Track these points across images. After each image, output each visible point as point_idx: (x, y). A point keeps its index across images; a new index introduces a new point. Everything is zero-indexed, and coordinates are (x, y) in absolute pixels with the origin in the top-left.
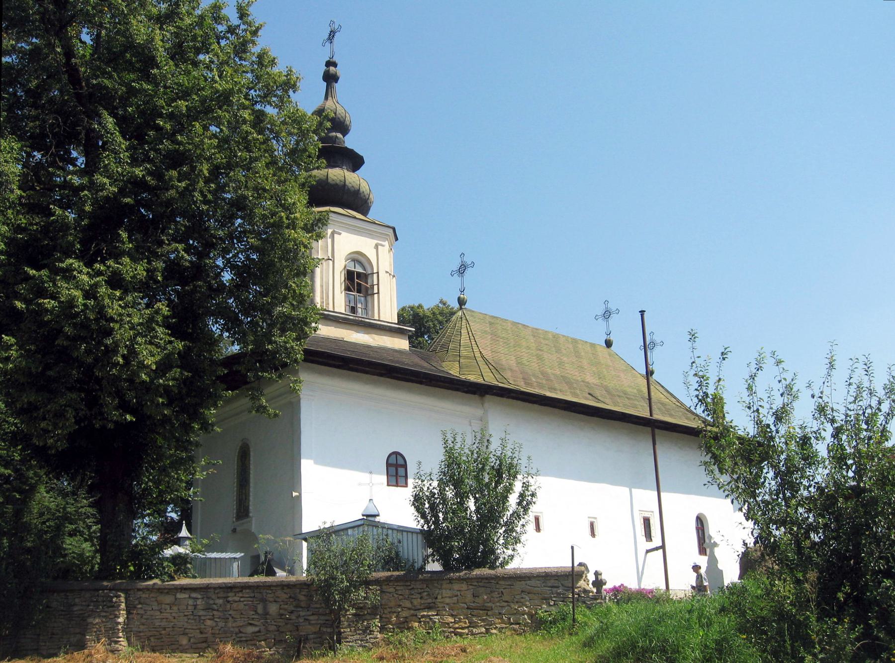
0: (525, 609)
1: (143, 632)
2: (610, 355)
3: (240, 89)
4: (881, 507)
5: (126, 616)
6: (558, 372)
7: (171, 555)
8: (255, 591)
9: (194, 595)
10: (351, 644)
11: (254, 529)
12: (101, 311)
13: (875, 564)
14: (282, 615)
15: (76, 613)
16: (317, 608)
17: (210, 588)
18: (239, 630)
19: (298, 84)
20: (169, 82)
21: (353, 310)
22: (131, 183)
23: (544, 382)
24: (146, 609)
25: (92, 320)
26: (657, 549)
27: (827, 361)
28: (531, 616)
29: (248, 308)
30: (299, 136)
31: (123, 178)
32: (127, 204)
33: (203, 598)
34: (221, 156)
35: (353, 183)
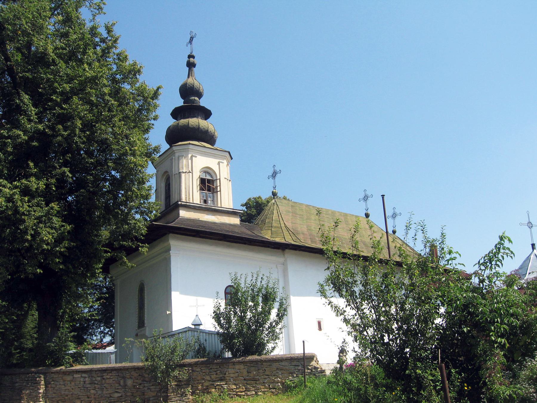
0: (279, 379)
5: (44, 389)
8: (119, 372)
9: (84, 375)
12: (16, 211)
14: (135, 386)
15: (17, 387)
17: (93, 371)
21: (205, 202)
24: (57, 384)
25: (11, 215)
28: (283, 384)
33: (89, 377)
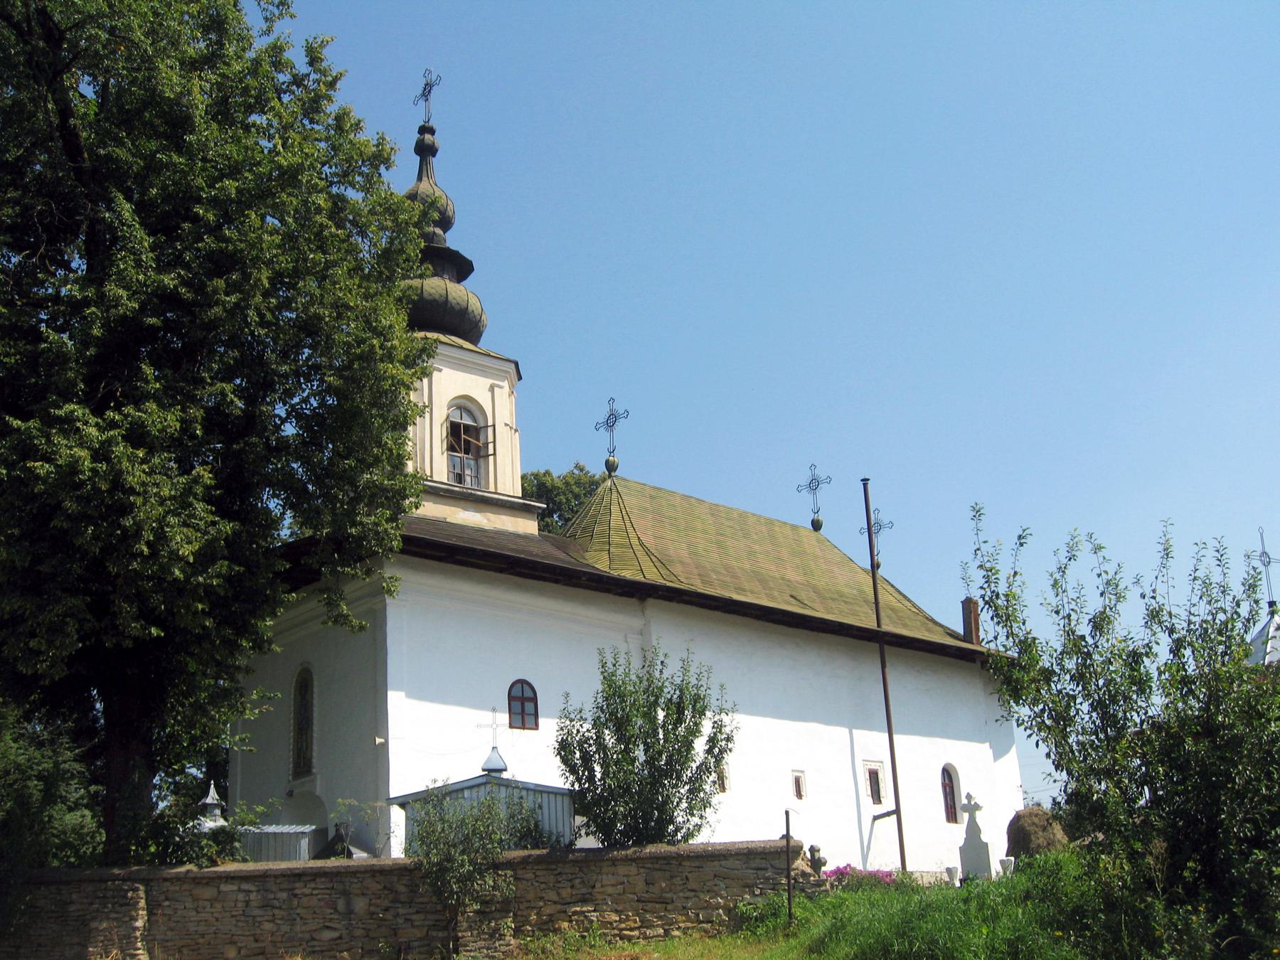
0: (720, 900)
1: (171, 940)
2: (818, 541)
3: (312, 164)
4: (1247, 749)
5: (146, 918)
6: (747, 566)
7: (210, 829)
8: (334, 880)
9: (245, 886)
10: (472, 954)
11: (319, 791)
13: (1239, 829)
14: (373, 913)
16: (423, 903)
17: (270, 876)
18: (311, 936)
19: (393, 158)
20: (211, 153)
21: (460, 478)
22: (157, 296)
23: (728, 579)
25: (104, 491)
26: (888, 814)
27: (1161, 548)
28: (728, 911)
29: (322, 475)
30: (393, 232)
31: (147, 289)
32: (152, 326)
33: (258, 891)
34: (286, 260)
35: (458, 299)
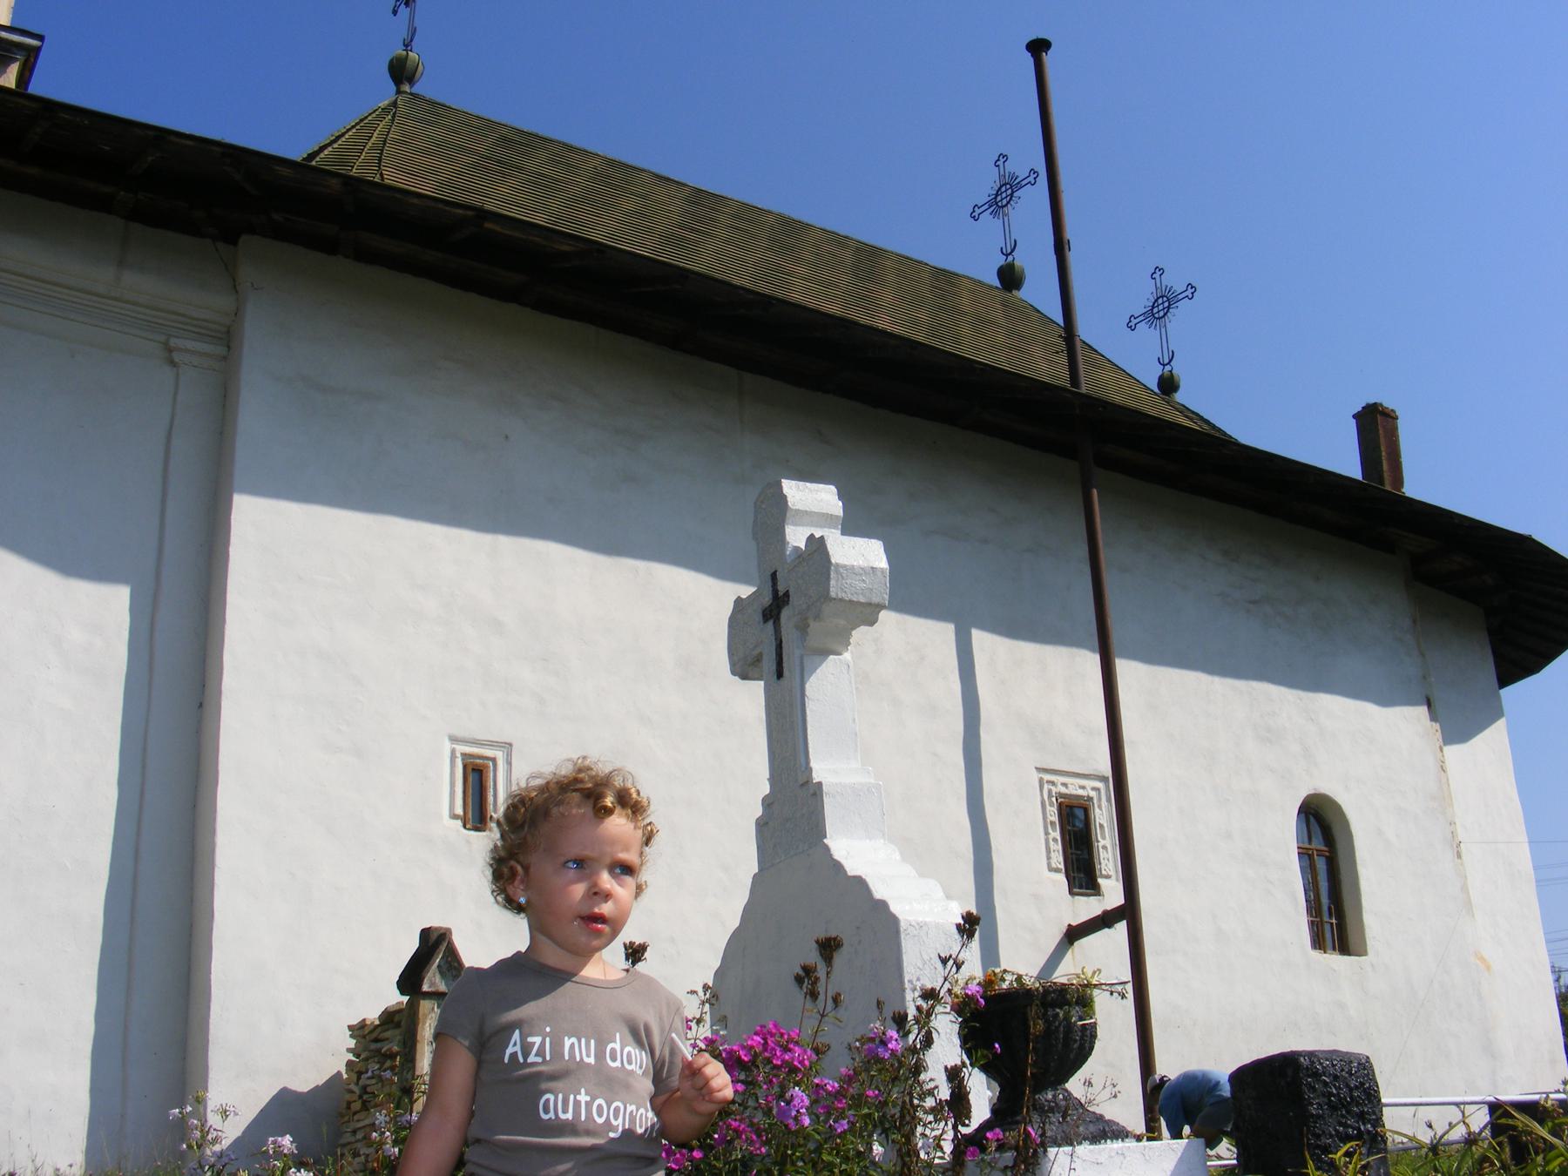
26: (1105, 921)
